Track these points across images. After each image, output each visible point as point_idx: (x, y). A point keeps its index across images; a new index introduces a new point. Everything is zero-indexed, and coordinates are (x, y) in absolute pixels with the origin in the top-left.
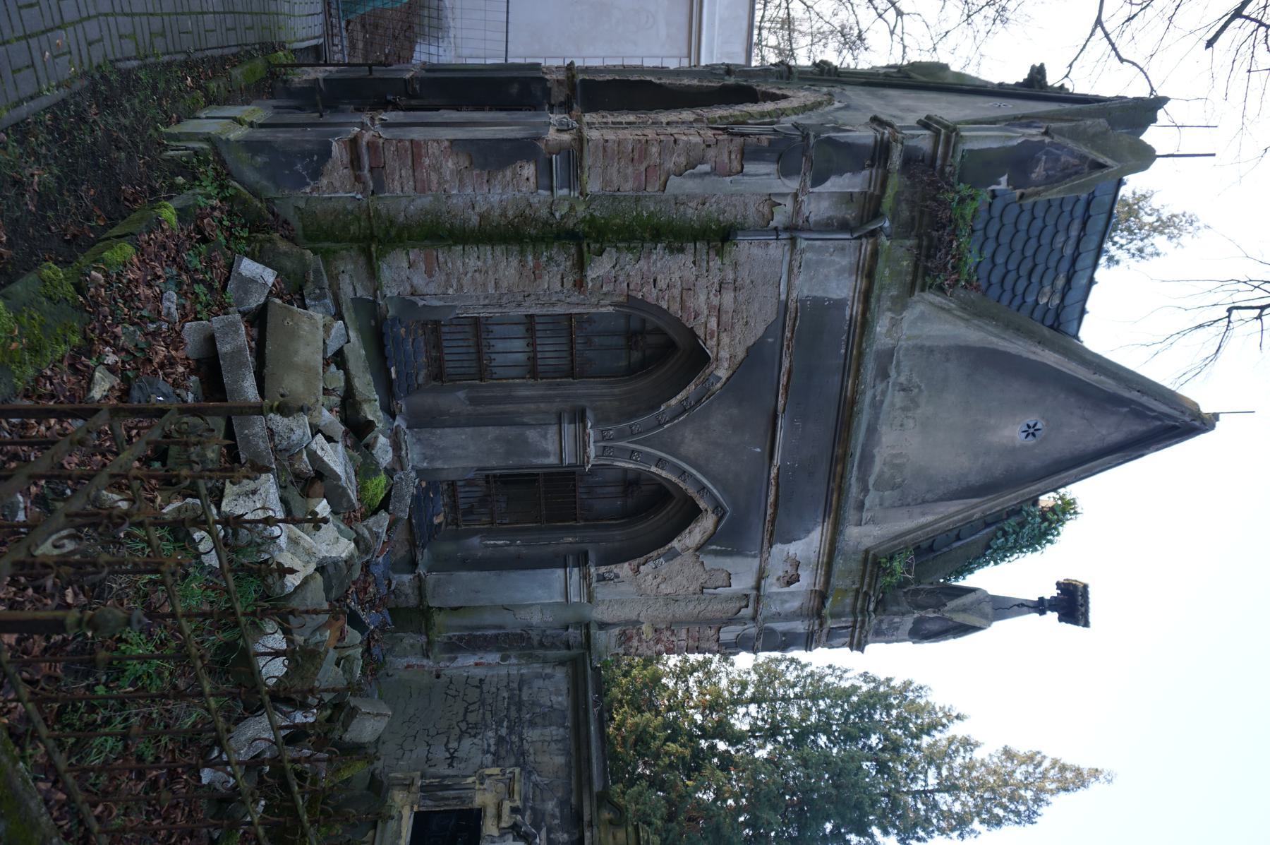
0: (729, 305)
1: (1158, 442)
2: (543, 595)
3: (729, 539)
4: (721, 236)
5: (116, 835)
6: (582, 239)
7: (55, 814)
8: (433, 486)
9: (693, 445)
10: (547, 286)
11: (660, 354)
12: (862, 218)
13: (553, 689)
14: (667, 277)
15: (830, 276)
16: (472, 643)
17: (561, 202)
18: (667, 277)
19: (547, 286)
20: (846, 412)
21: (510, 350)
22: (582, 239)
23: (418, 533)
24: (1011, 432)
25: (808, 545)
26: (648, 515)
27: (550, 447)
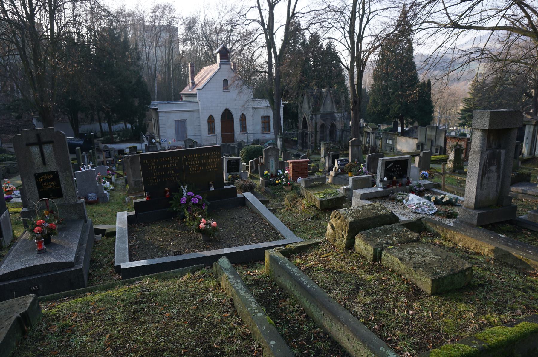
0: (320, 122)
1: (369, 219)
2: (338, 133)
3: (335, 120)
4: (316, 123)
5: (318, 352)
6: (316, 131)
7: (75, 217)
8: (330, 140)
9: (328, 124)
10: (319, 133)
11: (323, 126)
12: (316, 115)
13: (345, 132)
14: (318, 126)
15: (319, 116)
16: (342, 138)
17: (314, 133)
18: (318, 126)
19: (319, 133)
20: (327, 114)
21: (322, 135)
22: (316, 131)
23: (333, 141)
24: (329, 102)
25: (336, 115)
26: (333, 126)
27: (328, 132)
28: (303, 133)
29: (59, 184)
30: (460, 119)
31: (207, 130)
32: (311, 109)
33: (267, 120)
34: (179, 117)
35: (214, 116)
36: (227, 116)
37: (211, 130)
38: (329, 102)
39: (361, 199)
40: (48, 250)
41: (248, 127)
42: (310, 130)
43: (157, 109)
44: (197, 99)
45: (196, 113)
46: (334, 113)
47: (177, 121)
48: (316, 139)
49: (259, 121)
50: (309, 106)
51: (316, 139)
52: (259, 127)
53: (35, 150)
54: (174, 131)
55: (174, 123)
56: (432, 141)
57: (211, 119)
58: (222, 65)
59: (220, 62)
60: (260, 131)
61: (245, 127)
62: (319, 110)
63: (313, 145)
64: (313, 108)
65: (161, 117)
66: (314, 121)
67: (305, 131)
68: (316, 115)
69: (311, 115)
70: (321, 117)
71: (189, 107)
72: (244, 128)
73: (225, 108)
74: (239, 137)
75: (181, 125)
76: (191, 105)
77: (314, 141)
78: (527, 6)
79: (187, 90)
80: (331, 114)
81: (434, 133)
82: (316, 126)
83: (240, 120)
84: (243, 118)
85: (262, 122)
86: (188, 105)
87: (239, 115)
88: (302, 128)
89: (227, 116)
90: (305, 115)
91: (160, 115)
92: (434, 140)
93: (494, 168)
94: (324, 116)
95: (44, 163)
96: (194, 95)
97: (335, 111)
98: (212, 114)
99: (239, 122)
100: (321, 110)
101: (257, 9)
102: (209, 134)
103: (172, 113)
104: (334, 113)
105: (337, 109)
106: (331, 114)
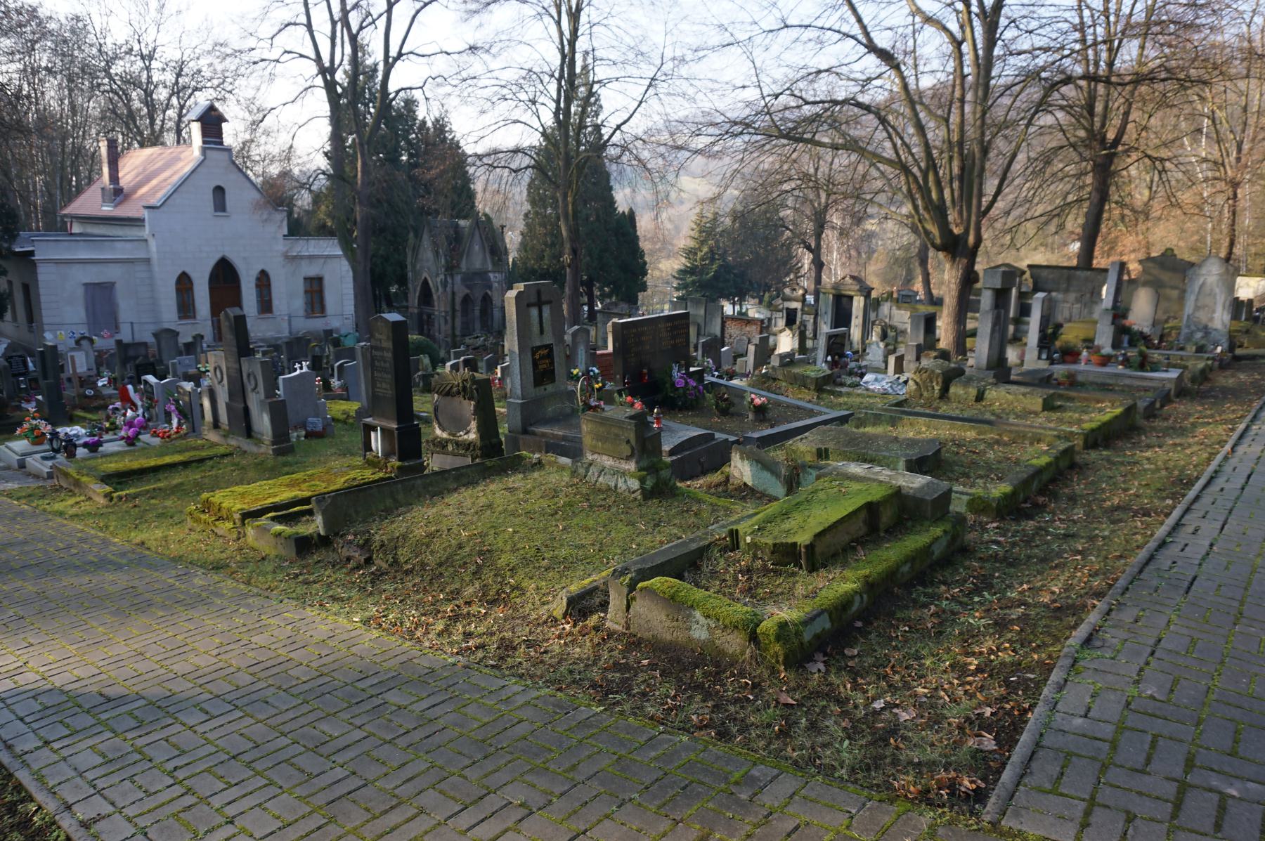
0: (461, 291)
3: (490, 287)
4: (453, 293)
6: (454, 310)
8: (482, 329)
9: (478, 295)
10: (459, 314)
11: (466, 300)
12: (452, 276)
15: (458, 278)
18: (458, 300)
19: (459, 314)
22: (454, 310)
24: (477, 248)
25: (491, 275)
27: (477, 313)
28: (420, 315)
29: (552, 363)
30: (677, 289)
32: (443, 261)
33: (316, 288)
34: (312, 271)
35: (193, 275)
36: (224, 275)
37: (186, 308)
38: (477, 248)
40: (1080, 345)
41: (275, 302)
42: (440, 306)
43: (32, 253)
44: (146, 232)
46: (486, 272)
47: (90, 287)
48: (453, 328)
49: (300, 287)
50: (437, 254)
51: (453, 328)
52: (299, 303)
53: (534, 312)
54: (82, 313)
55: (80, 292)
56: (699, 325)
57: (184, 283)
58: (208, 152)
59: (204, 142)
60: (302, 312)
61: (270, 301)
62: (458, 266)
63: (449, 339)
64: (447, 261)
65: (45, 275)
66: (449, 289)
67: (427, 310)
68: (452, 276)
69: (442, 277)
70: (463, 280)
71: (122, 251)
72: (266, 306)
73: (217, 257)
74: (259, 329)
75: (100, 299)
76: (128, 245)
77: (450, 332)
79: (90, 202)
80: (483, 274)
81: (702, 312)
82: (453, 299)
83: (257, 286)
84: (264, 280)
85: (306, 292)
86: (119, 245)
87: (255, 273)
88: (419, 304)
89: (224, 275)
90: (425, 275)
91: (41, 269)
92: (702, 325)
94: (469, 279)
95: (542, 332)
96: (137, 222)
97: (490, 267)
98: (188, 271)
100: (463, 266)
101: (302, 30)
102: (180, 318)
103: (78, 266)
104: (486, 272)
105: (494, 264)
106: (483, 274)
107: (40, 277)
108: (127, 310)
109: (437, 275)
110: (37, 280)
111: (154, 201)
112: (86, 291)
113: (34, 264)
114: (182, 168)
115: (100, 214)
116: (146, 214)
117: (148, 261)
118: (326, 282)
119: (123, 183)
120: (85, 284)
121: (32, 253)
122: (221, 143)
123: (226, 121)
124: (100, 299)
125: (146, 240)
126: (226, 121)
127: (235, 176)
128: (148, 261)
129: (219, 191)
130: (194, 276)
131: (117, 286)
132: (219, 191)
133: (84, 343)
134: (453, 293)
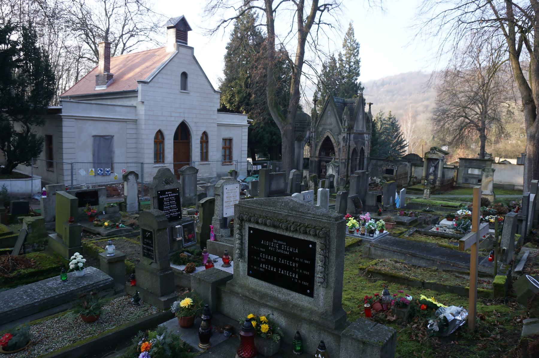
4: (349, 146)
11: (355, 150)
26: (362, 151)
31: (152, 155)
34: (227, 135)
36: (183, 132)
37: (159, 156)
39: (468, 297)
41: (210, 154)
45: (133, 126)
55: (90, 141)
57: (159, 137)
59: (177, 42)
61: (207, 153)
65: (67, 127)
72: (204, 156)
75: (103, 146)
78: (301, 20)
84: (205, 138)
85: (223, 148)
87: (200, 133)
89: (183, 132)
90: (327, 134)
93: (480, 124)
99: (199, 146)
107: (64, 129)
108: (121, 155)
109: (340, 133)
110: (61, 132)
111: (145, 78)
112: (94, 140)
113: (60, 119)
114: (160, 59)
115: (95, 92)
116: (140, 87)
117: (135, 121)
118: (234, 142)
119: (112, 71)
120: (94, 136)
121: (59, 111)
122: (186, 44)
123: (190, 29)
124: (103, 146)
125: (135, 107)
126: (190, 29)
127: (194, 66)
128: (135, 121)
129: (184, 75)
130: (165, 133)
131: (115, 138)
132: (184, 75)
133: (131, 177)
134: (349, 146)
